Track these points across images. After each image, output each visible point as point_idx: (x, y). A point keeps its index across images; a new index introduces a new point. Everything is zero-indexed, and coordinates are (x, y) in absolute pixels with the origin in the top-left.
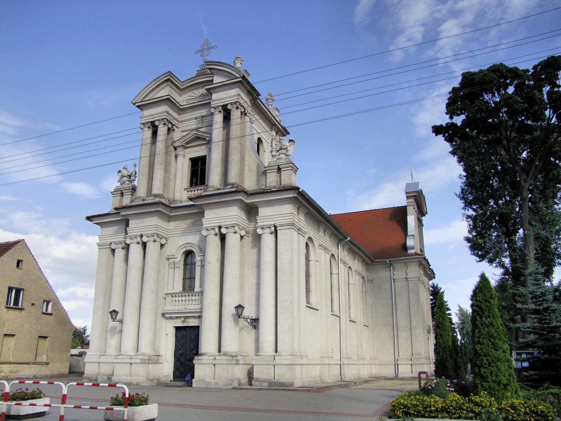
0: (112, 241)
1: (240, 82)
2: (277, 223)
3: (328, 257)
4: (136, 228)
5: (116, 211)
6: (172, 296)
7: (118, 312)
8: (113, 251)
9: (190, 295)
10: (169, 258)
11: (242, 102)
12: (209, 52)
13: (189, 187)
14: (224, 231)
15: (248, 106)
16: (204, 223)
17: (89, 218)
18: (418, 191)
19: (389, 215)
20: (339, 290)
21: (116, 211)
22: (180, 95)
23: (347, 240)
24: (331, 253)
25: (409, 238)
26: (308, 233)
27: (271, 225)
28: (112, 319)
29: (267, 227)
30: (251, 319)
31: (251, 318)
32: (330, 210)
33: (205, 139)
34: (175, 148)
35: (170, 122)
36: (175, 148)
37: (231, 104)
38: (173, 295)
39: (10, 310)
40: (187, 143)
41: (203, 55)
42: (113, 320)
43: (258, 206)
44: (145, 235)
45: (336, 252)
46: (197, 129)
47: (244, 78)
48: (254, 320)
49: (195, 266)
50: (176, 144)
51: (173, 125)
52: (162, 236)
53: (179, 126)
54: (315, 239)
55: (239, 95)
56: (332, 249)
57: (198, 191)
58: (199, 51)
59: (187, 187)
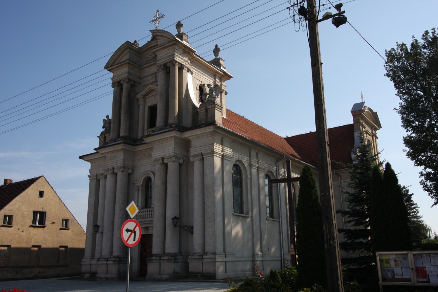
5: (95, 151)
12: (159, 21)
15: (183, 61)
16: (153, 156)
17: (81, 157)
19: (122, 161)
21: (95, 151)
39: (36, 228)
41: (156, 23)
43: (191, 140)
58: (153, 21)
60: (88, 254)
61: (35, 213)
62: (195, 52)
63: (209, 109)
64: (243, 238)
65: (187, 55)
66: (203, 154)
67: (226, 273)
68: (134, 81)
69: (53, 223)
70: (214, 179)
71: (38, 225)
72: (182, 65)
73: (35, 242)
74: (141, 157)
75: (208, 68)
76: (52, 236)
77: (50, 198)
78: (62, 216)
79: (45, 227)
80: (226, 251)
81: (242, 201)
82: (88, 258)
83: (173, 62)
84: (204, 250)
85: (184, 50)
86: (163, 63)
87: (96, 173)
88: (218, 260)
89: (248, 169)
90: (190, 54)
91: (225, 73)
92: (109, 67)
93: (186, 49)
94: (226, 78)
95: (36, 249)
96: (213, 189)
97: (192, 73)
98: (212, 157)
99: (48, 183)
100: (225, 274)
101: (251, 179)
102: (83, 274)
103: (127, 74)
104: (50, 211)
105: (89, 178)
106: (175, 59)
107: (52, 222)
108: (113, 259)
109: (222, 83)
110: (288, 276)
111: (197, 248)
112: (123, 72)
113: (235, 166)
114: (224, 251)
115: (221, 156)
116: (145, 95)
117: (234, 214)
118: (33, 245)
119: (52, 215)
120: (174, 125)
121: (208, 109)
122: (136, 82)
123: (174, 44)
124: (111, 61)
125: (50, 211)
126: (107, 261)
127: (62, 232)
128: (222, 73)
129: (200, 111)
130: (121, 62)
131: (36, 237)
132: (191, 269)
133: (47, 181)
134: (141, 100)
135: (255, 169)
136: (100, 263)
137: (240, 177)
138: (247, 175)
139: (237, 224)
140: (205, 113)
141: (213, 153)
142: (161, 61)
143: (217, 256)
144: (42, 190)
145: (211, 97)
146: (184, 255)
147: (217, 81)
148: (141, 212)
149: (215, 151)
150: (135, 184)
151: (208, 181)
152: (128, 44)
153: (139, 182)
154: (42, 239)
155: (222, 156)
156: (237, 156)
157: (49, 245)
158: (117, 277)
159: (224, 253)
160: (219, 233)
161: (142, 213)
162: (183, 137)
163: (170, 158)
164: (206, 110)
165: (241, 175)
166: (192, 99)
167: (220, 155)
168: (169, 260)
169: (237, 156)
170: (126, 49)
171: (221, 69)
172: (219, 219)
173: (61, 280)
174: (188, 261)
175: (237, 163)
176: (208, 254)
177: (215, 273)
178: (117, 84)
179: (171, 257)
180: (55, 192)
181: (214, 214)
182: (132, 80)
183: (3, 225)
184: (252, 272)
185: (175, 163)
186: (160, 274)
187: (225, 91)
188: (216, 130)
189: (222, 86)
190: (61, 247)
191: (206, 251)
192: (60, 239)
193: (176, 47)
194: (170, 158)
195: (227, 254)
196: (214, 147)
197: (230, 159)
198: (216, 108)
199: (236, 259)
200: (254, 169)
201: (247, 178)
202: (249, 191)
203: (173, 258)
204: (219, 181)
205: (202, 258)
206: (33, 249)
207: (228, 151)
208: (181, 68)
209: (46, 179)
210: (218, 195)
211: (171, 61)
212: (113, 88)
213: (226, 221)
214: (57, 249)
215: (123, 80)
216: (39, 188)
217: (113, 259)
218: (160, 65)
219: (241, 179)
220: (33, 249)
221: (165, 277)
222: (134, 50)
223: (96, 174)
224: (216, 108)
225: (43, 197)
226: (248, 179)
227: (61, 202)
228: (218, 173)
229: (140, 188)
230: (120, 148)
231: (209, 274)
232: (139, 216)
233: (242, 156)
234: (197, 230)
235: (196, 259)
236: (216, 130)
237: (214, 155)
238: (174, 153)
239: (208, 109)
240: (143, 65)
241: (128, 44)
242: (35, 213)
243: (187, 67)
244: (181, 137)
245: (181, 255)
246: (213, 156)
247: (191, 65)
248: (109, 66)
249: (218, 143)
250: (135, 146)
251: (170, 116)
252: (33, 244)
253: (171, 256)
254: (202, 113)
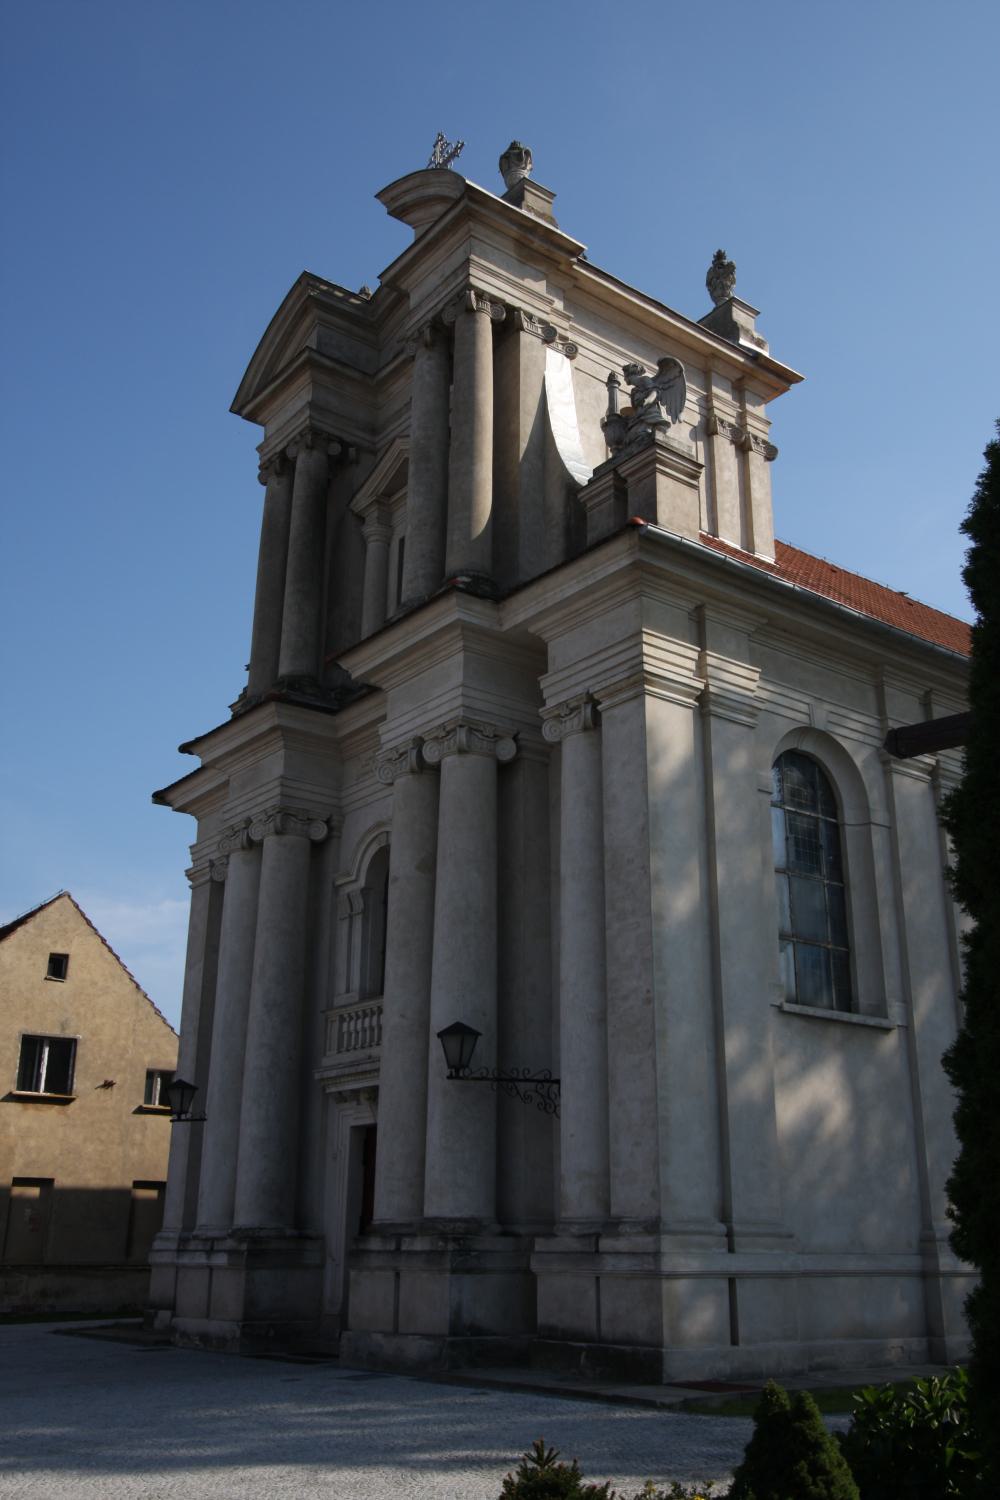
28: (450, 1066)
39: (30, 1106)
60: (173, 1216)
61: (31, 1045)
62: (582, 249)
63: (630, 480)
64: (858, 1140)
65: (542, 269)
66: (596, 697)
67: (734, 1341)
68: (341, 442)
69: (108, 1085)
70: (646, 814)
71: (42, 1092)
72: (511, 310)
73: (27, 1165)
74: (367, 765)
75: (664, 335)
76: (102, 1142)
77: (94, 983)
78: (147, 1058)
79: (73, 1100)
80: (738, 1209)
81: (847, 946)
82: (171, 1235)
83: (462, 301)
84: (607, 1205)
85: (521, 245)
86: (429, 316)
87: (208, 858)
88: (673, 1261)
89: (870, 776)
90: (559, 263)
91: (756, 357)
92: (249, 404)
93: (530, 237)
94: (767, 385)
95: (34, 1192)
96: (646, 868)
97: (571, 352)
98: (634, 703)
99: (89, 923)
100: (728, 1347)
101: (891, 829)
102: (152, 1311)
103: (308, 413)
104: (93, 1035)
105: (190, 883)
106: (473, 280)
107: (102, 1083)
108: (230, 1244)
109: (749, 407)
110: (949, 1451)
111: (576, 1199)
112: (295, 404)
113: (790, 759)
114: (725, 1215)
115: (691, 701)
116: (389, 493)
117: (787, 1007)
118: (16, 1175)
119: (104, 1053)
120: (467, 576)
121: (625, 481)
122: (352, 446)
123: (468, 215)
124: (255, 376)
125: (93, 1035)
126: (210, 1252)
127: (144, 1123)
128: (742, 360)
129: (591, 499)
130: (278, 371)
131: (32, 1143)
132: (548, 1312)
133: (83, 915)
134: (373, 515)
135: (917, 778)
136: (186, 1260)
137: (833, 820)
138: (865, 808)
139: (807, 1065)
140: (612, 500)
141: (637, 681)
142: (422, 313)
143: (667, 1243)
144: (59, 950)
145: (642, 421)
146: (522, 1230)
147: (718, 397)
148: (351, 1018)
149: (647, 667)
150: (341, 886)
151: (621, 830)
152: (308, 284)
153: (353, 878)
154: (57, 1152)
155: (698, 699)
156: (803, 708)
157: (89, 1175)
158: (238, 1333)
159: (722, 1228)
160: (686, 1111)
161: (360, 1022)
162: (506, 627)
163: (448, 733)
164: (617, 489)
165: (832, 806)
166: (563, 458)
167: (689, 695)
168: (432, 1257)
169: (803, 708)
170: (304, 312)
171: (741, 346)
172: (683, 1033)
173: (69, 1333)
174: (535, 1266)
175: (807, 746)
176: (622, 1228)
177: (660, 1344)
178: (277, 466)
179: (441, 1243)
180: (118, 958)
181: (649, 1001)
182: (330, 438)
183: (145, 1106)
184: (924, 1340)
185: (471, 759)
186: (396, 1332)
187: (764, 442)
188: (646, 558)
189: (749, 420)
190: (138, 1184)
191: (614, 1211)
192: (134, 1153)
193: (478, 230)
194: (448, 733)
195: (737, 1228)
196: (646, 649)
197: (752, 715)
198: (658, 466)
199: (807, 1263)
200: (907, 781)
201: (867, 824)
202: (884, 892)
203: (451, 1246)
204: (679, 829)
205: (597, 1251)
206: (17, 1191)
207: (739, 676)
208: (508, 327)
209: (77, 907)
210: (680, 901)
211: (458, 295)
212: (265, 488)
213: (733, 1046)
214: (122, 1193)
215: (296, 443)
216: (47, 941)
217: (230, 1244)
218: (418, 330)
219: (836, 831)
220: (17, 1191)
221: (414, 1348)
222: (343, 314)
223: (211, 861)
224: (658, 466)
225: (64, 978)
226: (873, 827)
227: (140, 997)
228: (679, 783)
229: (359, 904)
230: (265, 727)
231: (628, 1348)
232: (350, 1034)
233: (827, 707)
234: (575, 1100)
235: (565, 1254)
236: (646, 558)
237: (642, 694)
238: (463, 706)
239: (625, 481)
240: (380, 370)
241: (308, 284)
242: (31, 1045)
243: (541, 321)
244: (496, 628)
245: (504, 1234)
246: (641, 695)
247: (568, 318)
248: (251, 396)
249: (671, 630)
250: (332, 712)
251: (454, 537)
252: (18, 1170)
253: (443, 1236)
254: (600, 503)
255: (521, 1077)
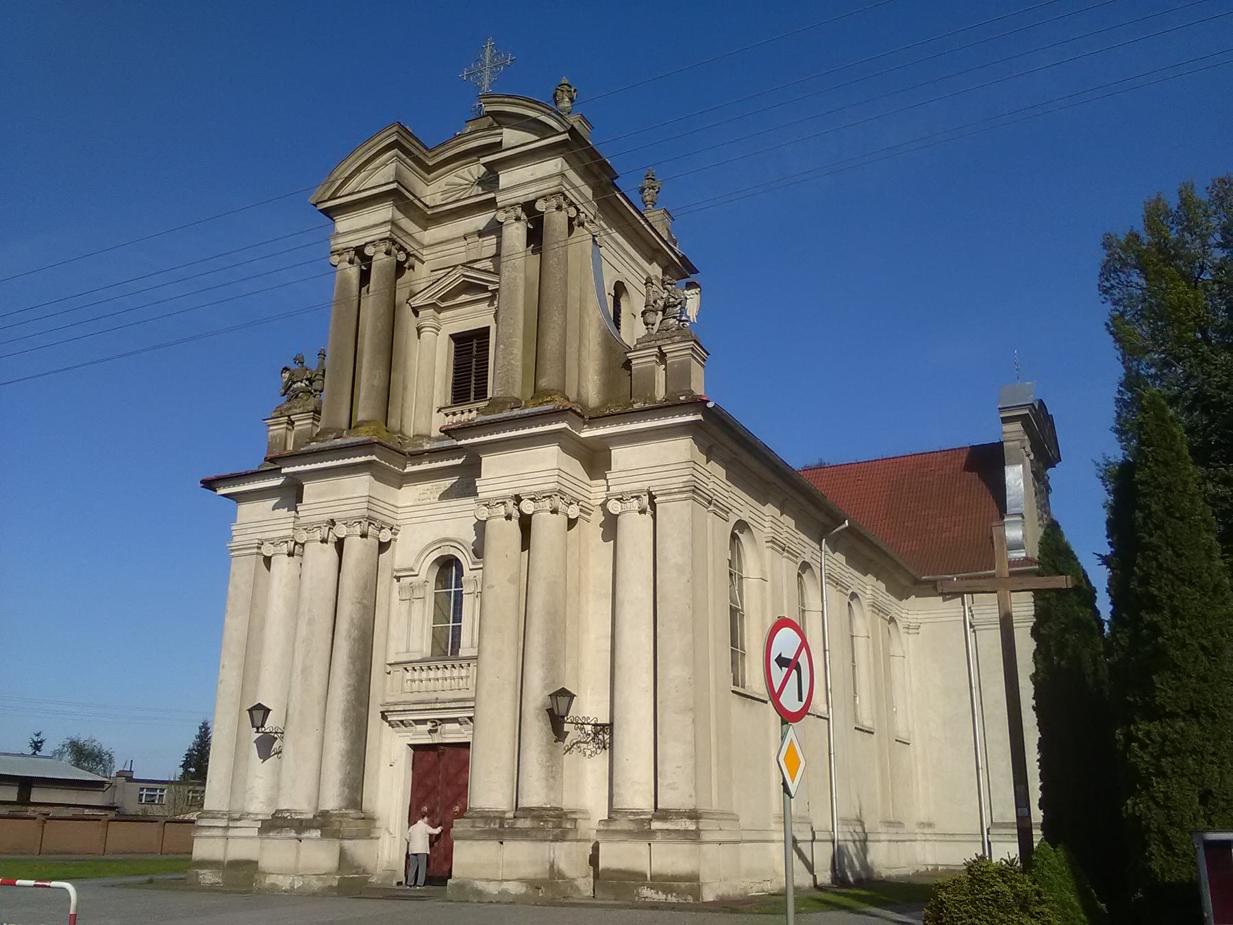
0: (267, 536)
1: (565, 142)
2: (655, 488)
3: (795, 569)
4: (318, 506)
6: (406, 669)
7: (269, 710)
8: (268, 561)
9: (449, 666)
10: (400, 577)
11: (572, 195)
13: (449, 404)
14: (527, 507)
18: (1032, 404)
20: (825, 651)
22: (427, 182)
23: (843, 527)
24: (800, 561)
25: (1011, 522)
26: (734, 510)
27: (642, 491)
29: (632, 497)
30: (595, 725)
31: (593, 722)
32: (795, 457)
33: (485, 289)
34: (416, 311)
35: (402, 248)
36: (416, 311)
37: (544, 197)
38: (405, 665)
40: (443, 299)
42: (255, 729)
44: (340, 520)
45: (814, 556)
46: (468, 263)
47: (161, 798)
48: (603, 725)
49: (462, 595)
50: (417, 302)
51: (408, 255)
52: (383, 522)
53: (424, 258)
54: (755, 524)
55: (562, 175)
56: (804, 549)
57: (469, 414)
59: (443, 405)
255: (586, 722)
